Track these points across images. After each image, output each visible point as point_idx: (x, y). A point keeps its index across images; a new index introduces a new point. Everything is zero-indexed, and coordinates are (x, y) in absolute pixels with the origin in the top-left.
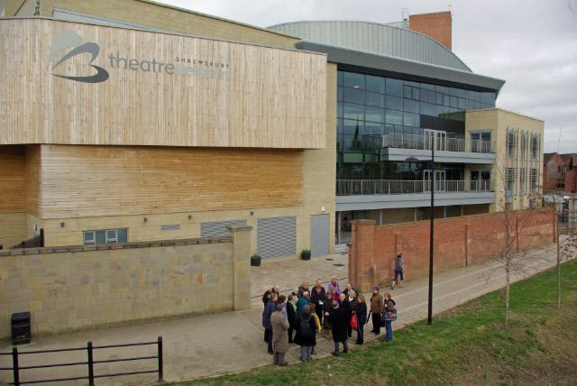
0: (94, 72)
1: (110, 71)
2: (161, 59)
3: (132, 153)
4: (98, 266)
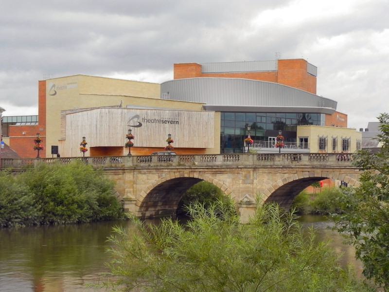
3: (147, 149)
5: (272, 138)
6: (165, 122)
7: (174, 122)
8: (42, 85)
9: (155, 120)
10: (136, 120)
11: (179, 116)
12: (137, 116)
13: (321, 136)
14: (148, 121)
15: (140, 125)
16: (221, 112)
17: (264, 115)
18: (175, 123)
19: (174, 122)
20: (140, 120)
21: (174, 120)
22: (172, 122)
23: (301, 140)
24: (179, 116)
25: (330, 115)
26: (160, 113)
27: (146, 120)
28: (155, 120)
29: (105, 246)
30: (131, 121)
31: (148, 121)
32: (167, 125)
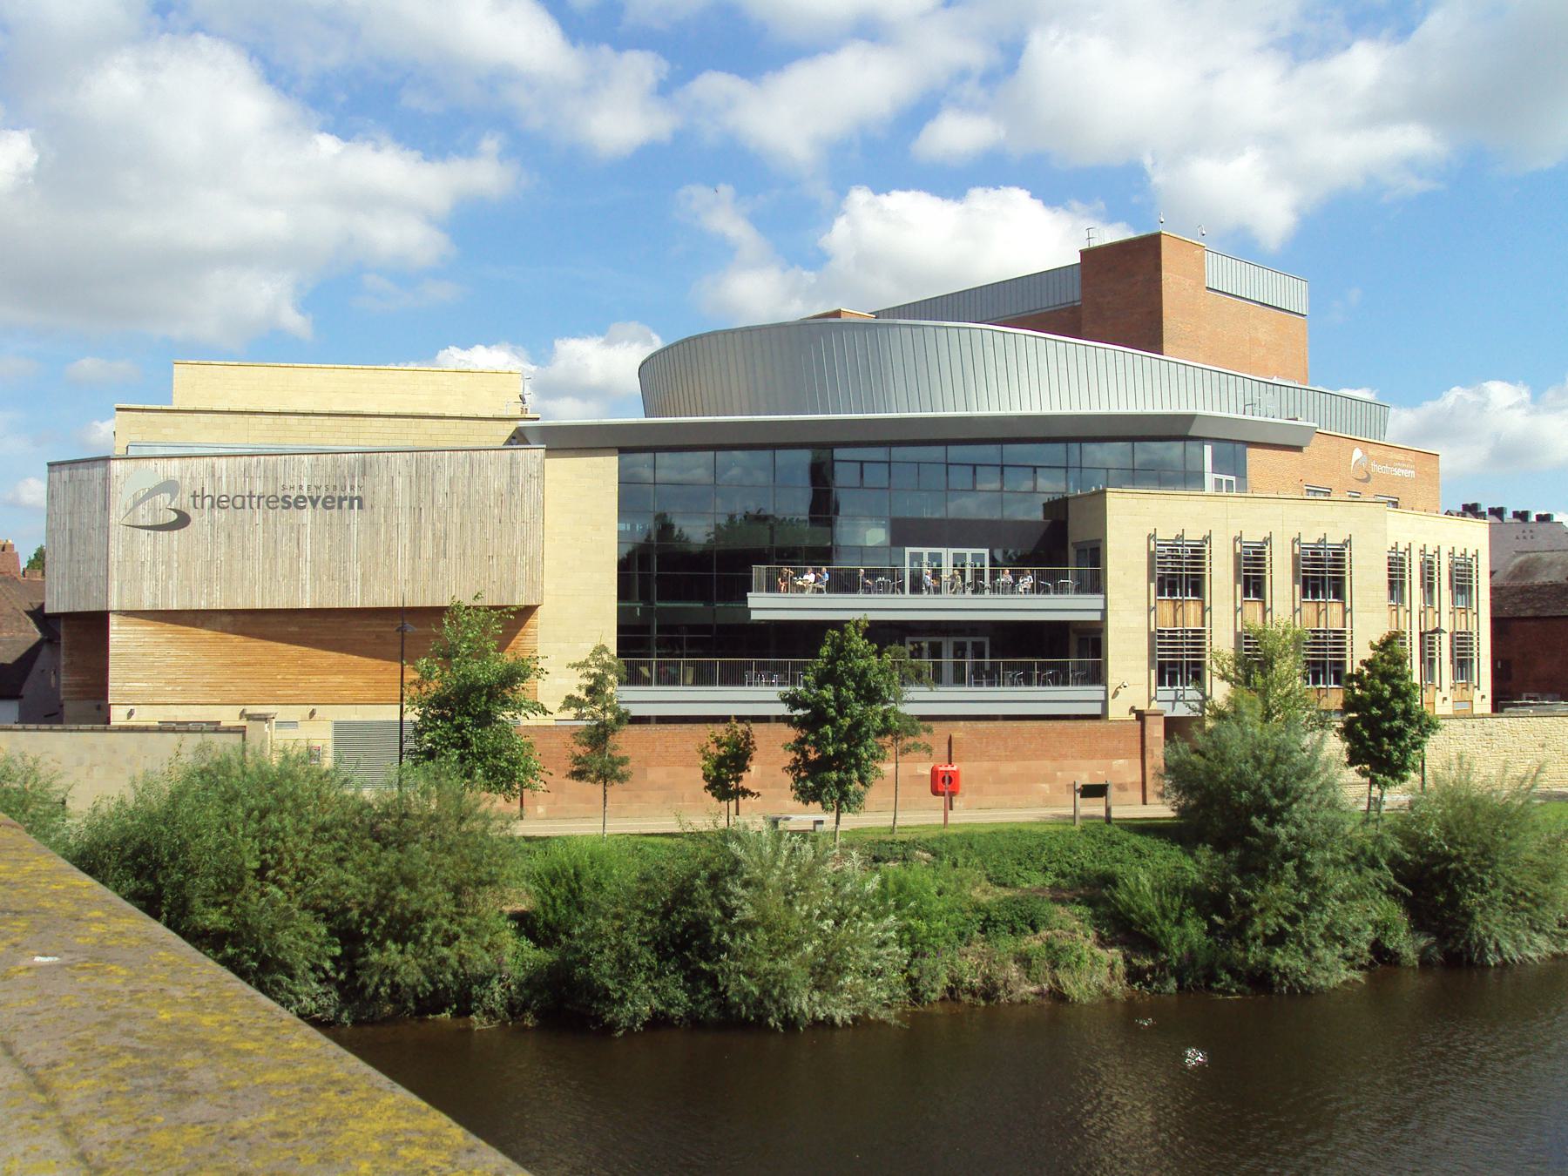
0: (174, 516)
1: (192, 513)
2: (259, 489)
4: (93, 747)
5: (926, 551)
6: (299, 502)
7: (341, 500)
8: (1144, 803)
9: (251, 496)
10: (163, 499)
11: (364, 474)
12: (170, 486)
13: (1310, 538)
14: (217, 503)
15: (183, 520)
16: (622, 450)
17: (879, 453)
18: (346, 504)
19: (341, 500)
20: (184, 502)
21: (337, 494)
22: (332, 502)
23: (1080, 551)
24: (364, 474)
25: (1298, 449)
26: (275, 465)
27: (208, 501)
28: (251, 496)
29: (371, 792)
30: (141, 510)
31: (217, 503)
32: (307, 514)
